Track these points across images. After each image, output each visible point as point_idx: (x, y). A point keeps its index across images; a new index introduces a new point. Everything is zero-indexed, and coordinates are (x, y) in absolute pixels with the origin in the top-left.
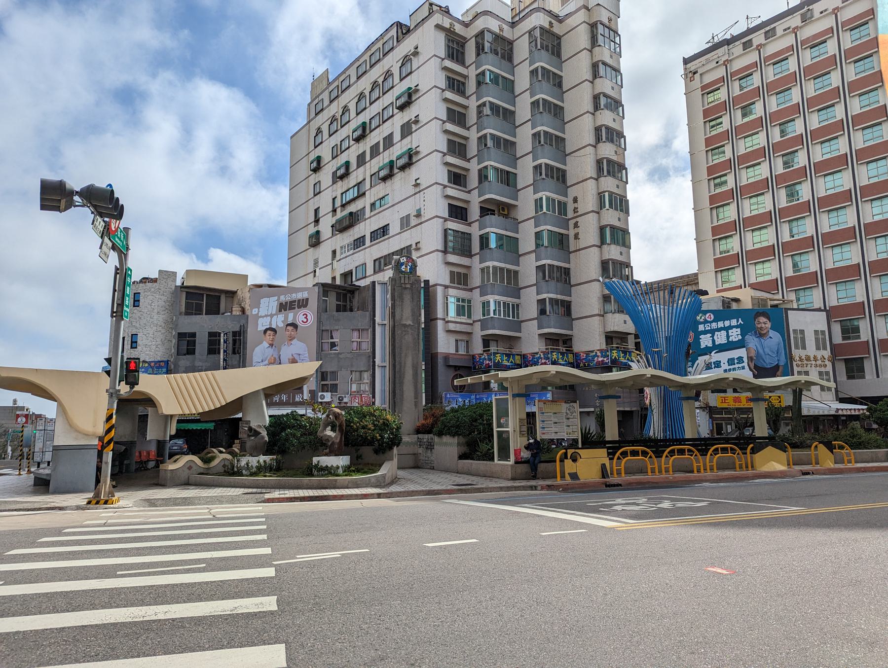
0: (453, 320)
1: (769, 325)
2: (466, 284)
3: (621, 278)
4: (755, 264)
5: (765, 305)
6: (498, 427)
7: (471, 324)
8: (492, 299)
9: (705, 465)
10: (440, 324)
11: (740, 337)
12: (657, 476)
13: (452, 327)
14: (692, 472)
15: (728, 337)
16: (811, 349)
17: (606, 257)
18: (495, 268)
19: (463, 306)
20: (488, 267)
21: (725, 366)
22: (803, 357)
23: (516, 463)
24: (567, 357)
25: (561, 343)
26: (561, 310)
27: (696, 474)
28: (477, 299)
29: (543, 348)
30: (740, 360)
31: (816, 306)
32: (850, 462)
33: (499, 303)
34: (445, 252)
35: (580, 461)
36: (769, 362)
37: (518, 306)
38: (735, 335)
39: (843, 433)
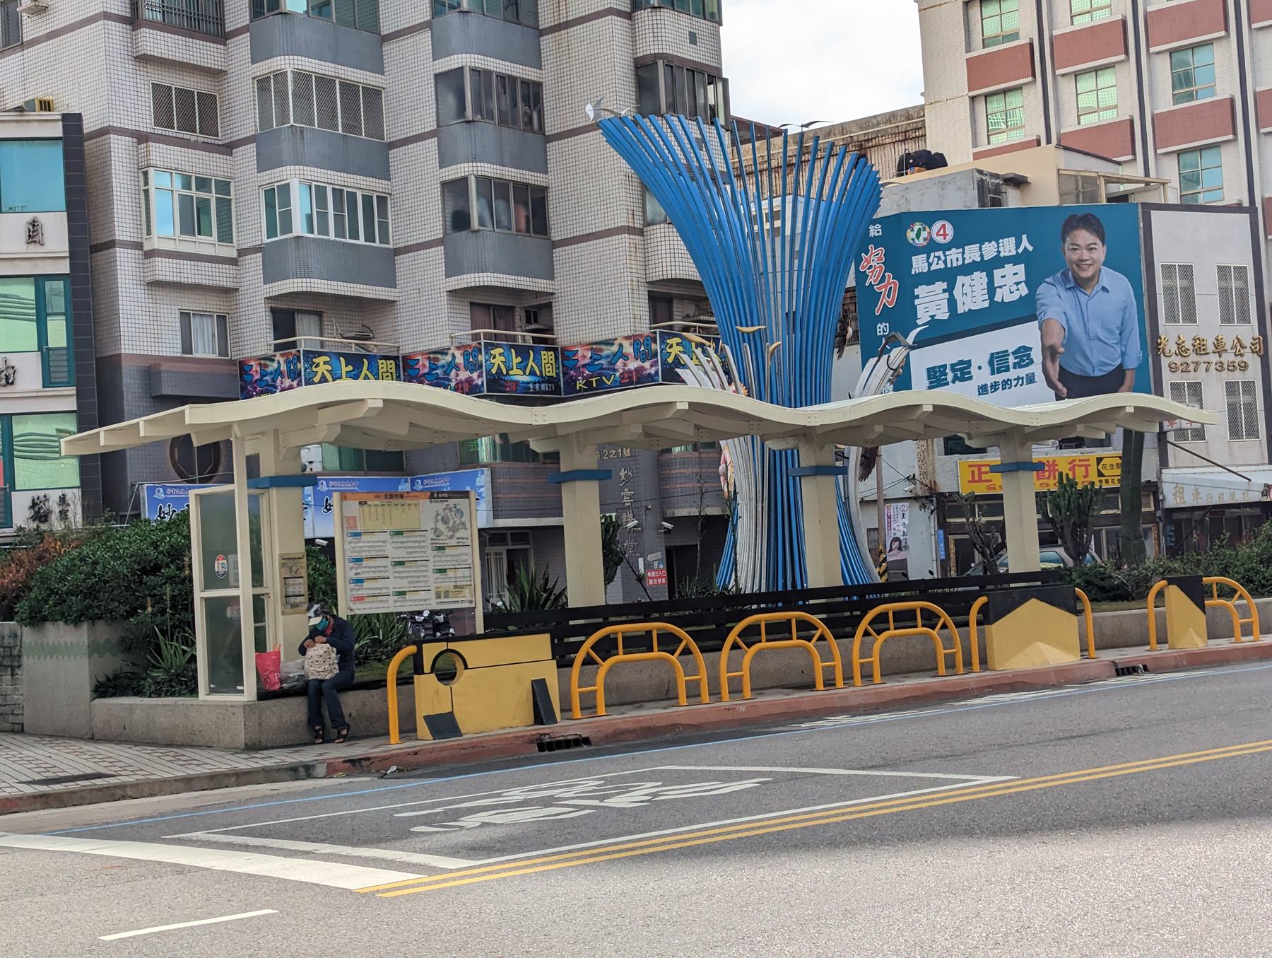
0: (170, 246)
1: (1100, 253)
2: (209, 127)
3: (693, 115)
4: (1076, 75)
5: (1094, 197)
6: (208, 585)
7: (233, 262)
8: (299, 181)
9: (848, 666)
10: (125, 264)
11: (1024, 291)
12: (705, 709)
13: (165, 270)
14: (811, 686)
15: (991, 289)
16: (1208, 321)
17: (647, 48)
18: (302, 78)
19: (204, 204)
20: (280, 76)
21: (982, 375)
22: (1188, 345)
23: (263, 695)
24: (537, 360)
25: (519, 316)
26: (518, 216)
27: (820, 692)
28: (248, 178)
29: (465, 333)
30: (1023, 355)
31: (1230, 199)
32: (1247, 631)
33: (321, 192)
34: (133, 20)
35: (464, 676)
36: (1099, 361)
37: (382, 200)
38: (1011, 283)
39: (1244, 550)
